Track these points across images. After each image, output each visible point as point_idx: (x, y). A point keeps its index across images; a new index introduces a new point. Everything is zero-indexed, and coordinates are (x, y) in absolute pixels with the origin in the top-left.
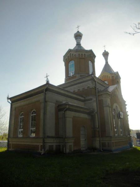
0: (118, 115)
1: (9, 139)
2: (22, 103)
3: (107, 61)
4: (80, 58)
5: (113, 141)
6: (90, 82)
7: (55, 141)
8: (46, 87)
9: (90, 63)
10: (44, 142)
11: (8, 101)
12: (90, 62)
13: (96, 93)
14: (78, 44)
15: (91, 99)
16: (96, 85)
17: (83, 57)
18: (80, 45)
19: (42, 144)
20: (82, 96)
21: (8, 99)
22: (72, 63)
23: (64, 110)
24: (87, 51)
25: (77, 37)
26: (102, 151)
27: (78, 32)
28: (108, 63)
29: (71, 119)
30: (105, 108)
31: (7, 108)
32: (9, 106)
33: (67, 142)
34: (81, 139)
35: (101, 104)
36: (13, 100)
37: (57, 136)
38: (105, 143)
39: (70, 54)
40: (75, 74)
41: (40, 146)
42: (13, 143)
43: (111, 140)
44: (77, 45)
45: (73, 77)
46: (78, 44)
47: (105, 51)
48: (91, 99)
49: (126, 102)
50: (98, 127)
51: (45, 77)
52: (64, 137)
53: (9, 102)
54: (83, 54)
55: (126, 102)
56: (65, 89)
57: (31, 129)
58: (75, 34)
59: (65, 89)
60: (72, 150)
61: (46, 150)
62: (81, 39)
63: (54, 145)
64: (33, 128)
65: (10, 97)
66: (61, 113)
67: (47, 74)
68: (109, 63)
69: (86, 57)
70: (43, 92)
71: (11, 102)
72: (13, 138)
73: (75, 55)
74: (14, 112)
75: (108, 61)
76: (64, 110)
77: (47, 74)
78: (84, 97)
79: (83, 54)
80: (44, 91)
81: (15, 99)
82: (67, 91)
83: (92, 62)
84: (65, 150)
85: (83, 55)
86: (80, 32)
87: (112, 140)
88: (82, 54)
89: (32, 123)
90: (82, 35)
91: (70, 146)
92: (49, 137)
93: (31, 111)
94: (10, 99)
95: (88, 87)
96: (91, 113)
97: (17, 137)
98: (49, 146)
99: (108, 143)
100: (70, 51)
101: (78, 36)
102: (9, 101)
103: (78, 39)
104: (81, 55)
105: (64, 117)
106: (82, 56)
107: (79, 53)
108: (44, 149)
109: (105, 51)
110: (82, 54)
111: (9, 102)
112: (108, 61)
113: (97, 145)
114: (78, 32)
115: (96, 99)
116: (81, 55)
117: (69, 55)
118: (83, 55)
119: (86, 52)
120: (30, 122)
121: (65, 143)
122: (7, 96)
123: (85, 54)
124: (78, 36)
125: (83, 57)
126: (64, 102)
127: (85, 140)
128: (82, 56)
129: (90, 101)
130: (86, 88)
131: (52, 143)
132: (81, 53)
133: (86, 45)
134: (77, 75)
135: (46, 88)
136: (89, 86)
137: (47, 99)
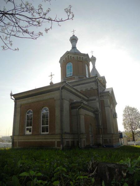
0: (114, 114)
1: (14, 137)
2: (30, 100)
3: (95, 66)
4: (78, 61)
5: (114, 138)
6: (94, 83)
7: (71, 137)
8: (61, 86)
10: (62, 139)
11: (11, 98)
12: (86, 65)
13: (98, 93)
14: (74, 48)
15: (95, 100)
16: (98, 87)
19: (59, 140)
20: (85, 96)
21: (11, 95)
22: (70, 65)
23: (78, 108)
24: (84, 55)
25: (73, 41)
26: (105, 147)
27: (74, 35)
29: (84, 116)
30: (106, 108)
31: (10, 105)
32: (12, 103)
33: (82, 138)
34: (11, 143)
35: (102, 104)
36: (17, 97)
37: (72, 133)
38: (107, 139)
39: (68, 56)
40: (73, 75)
41: (56, 142)
42: (20, 141)
43: (112, 137)
44: (73, 48)
45: (71, 78)
46: (74, 48)
48: (95, 100)
50: (101, 125)
51: (49, 76)
52: (79, 133)
53: (13, 99)
56: (74, 87)
57: (48, 125)
58: (71, 38)
59: (74, 87)
60: (86, 145)
61: (64, 145)
62: (76, 43)
63: (70, 140)
65: (13, 93)
66: (74, 111)
67: (51, 73)
68: (97, 68)
70: (59, 90)
71: (14, 99)
73: (73, 57)
74: (19, 109)
75: (95, 66)
76: (78, 108)
77: (51, 73)
78: (88, 97)
80: (60, 89)
81: (21, 96)
82: (75, 89)
83: (87, 65)
84: (81, 145)
85: (81, 58)
86: (75, 36)
89: (42, 120)
91: (84, 142)
92: (66, 133)
93: (27, 111)
94: (14, 95)
95: (91, 88)
96: (95, 112)
97: (24, 135)
98: (67, 141)
99: (110, 139)
100: (68, 53)
101: (74, 40)
102: (13, 97)
103: (74, 42)
104: (79, 58)
105: (78, 115)
106: (80, 59)
107: (77, 56)
108: (63, 144)
110: (80, 57)
111: (13, 99)
112: (96, 65)
113: (101, 142)
114: (74, 35)
115: (99, 99)
116: (79, 58)
117: (67, 57)
118: (81, 58)
119: (84, 56)
120: (41, 119)
121: (80, 138)
122: (10, 92)
123: (82, 58)
124: (74, 40)
125: (79, 59)
126: (75, 101)
127: (92, 136)
128: (80, 59)
129: (94, 101)
130: (89, 89)
131: (68, 139)
132: (79, 56)
133: (82, 48)
134: (76, 77)
135: (63, 86)
136: (92, 87)
137: (63, 97)
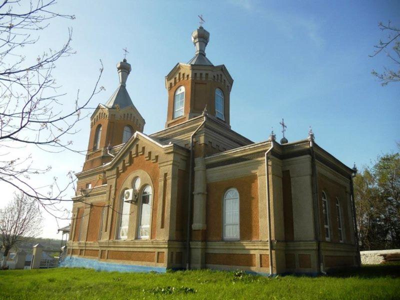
3: (125, 83)
9: (218, 93)
12: (217, 90)
17: (204, 79)
18: (204, 55)
28: (126, 88)
47: (125, 61)
49: (198, 29)
54: (204, 73)
55: (198, 29)
64: (89, 241)
68: (128, 88)
69: (209, 79)
72: (83, 250)
75: (126, 84)
79: (204, 73)
85: (204, 76)
87: (184, 156)
88: (201, 74)
90: (208, 34)
109: (125, 61)
112: (127, 83)
118: (204, 76)
125: (204, 79)
133: (215, 57)
